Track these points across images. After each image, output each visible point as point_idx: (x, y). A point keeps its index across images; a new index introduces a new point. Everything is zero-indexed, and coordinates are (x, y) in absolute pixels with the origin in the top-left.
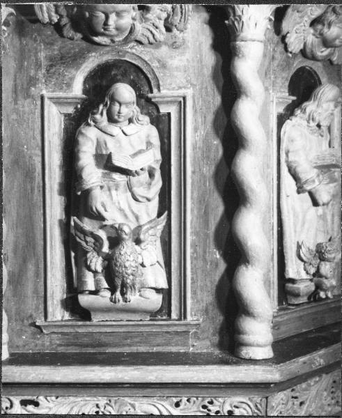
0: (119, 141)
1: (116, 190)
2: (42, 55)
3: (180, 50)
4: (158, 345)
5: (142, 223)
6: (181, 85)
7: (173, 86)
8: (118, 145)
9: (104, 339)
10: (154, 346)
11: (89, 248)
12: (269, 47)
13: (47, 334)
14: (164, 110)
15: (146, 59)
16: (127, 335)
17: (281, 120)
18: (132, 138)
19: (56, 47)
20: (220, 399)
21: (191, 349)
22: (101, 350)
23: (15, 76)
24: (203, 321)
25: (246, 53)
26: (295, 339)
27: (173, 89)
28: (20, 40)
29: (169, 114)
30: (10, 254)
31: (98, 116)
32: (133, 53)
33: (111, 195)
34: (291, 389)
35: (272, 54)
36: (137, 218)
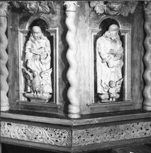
0: (37, 45)
1: (36, 60)
2: (18, 18)
3: (55, 15)
4: (49, 111)
5: (43, 71)
6: (55, 26)
7: (53, 26)
8: (36, 46)
9: (36, 108)
10: (48, 111)
11: (28, 79)
12: (87, 13)
13: (20, 105)
14: (52, 34)
15: (46, 18)
16: (41, 107)
17: (96, 38)
18: (40, 44)
19: (22, 15)
20: (58, 130)
21: (59, 113)
22: (34, 111)
23: (11, 24)
24: (62, 104)
25: (68, 16)
26: (99, 114)
27: (53, 28)
28: (13, 13)
29: (53, 36)
30: (11, 80)
31: (31, 37)
32: (43, 17)
33: (34, 62)
34: (86, 129)
35: (88, 15)
36: (42, 69)
